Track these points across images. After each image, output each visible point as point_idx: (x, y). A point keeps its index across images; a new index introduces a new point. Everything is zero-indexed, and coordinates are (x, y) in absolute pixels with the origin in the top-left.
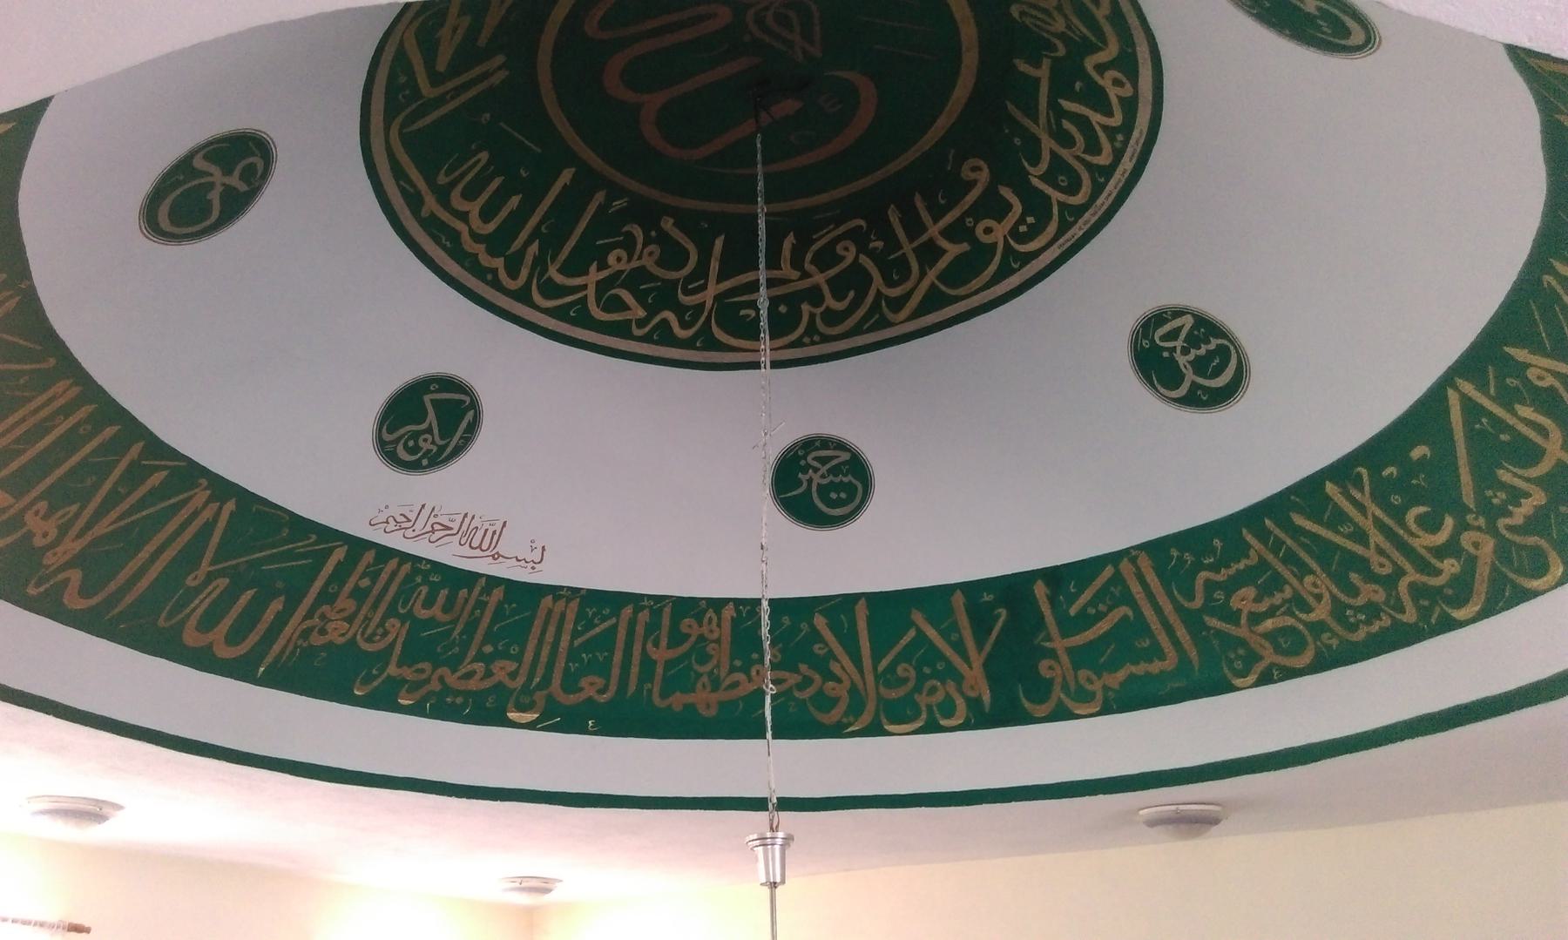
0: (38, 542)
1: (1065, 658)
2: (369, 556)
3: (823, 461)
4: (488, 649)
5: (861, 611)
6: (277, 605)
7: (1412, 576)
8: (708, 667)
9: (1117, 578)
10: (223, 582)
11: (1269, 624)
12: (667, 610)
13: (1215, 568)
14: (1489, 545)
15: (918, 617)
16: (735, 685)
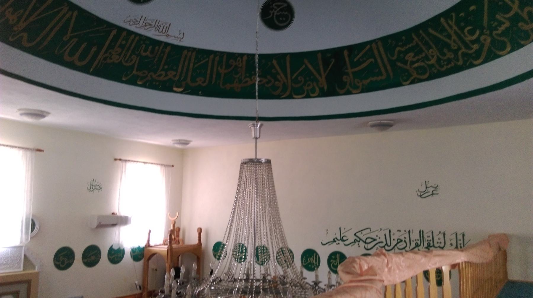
0: (11, 22)
1: (351, 75)
2: (124, 34)
3: (278, 6)
4: (166, 67)
5: (288, 58)
6: (94, 49)
7: (463, 50)
8: (238, 76)
9: (371, 49)
10: (76, 40)
11: (416, 65)
12: (225, 56)
13: (402, 46)
14: (489, 40)
15: (306, 61)
16: (247, 82)
